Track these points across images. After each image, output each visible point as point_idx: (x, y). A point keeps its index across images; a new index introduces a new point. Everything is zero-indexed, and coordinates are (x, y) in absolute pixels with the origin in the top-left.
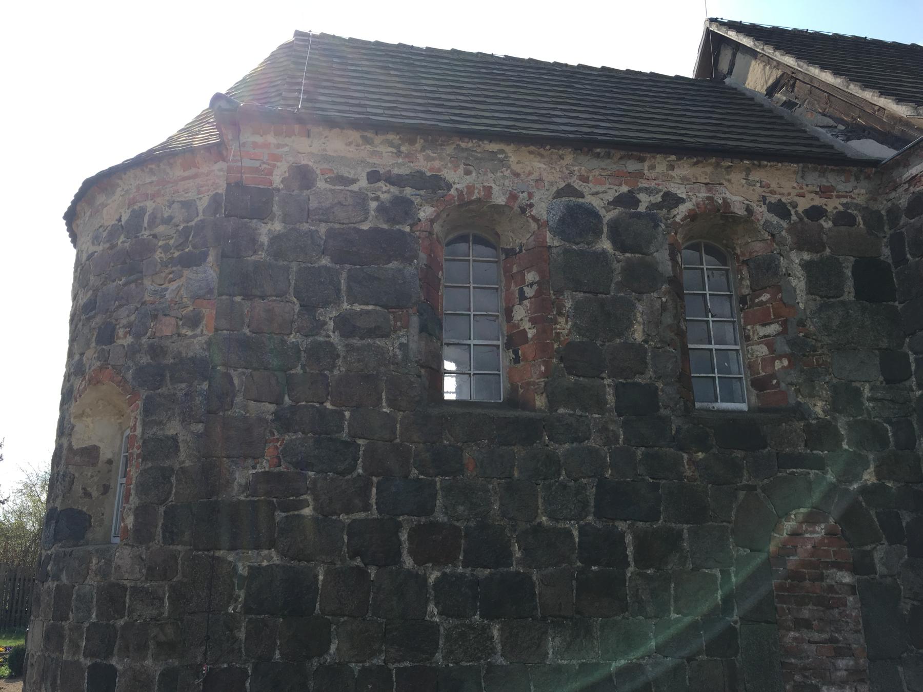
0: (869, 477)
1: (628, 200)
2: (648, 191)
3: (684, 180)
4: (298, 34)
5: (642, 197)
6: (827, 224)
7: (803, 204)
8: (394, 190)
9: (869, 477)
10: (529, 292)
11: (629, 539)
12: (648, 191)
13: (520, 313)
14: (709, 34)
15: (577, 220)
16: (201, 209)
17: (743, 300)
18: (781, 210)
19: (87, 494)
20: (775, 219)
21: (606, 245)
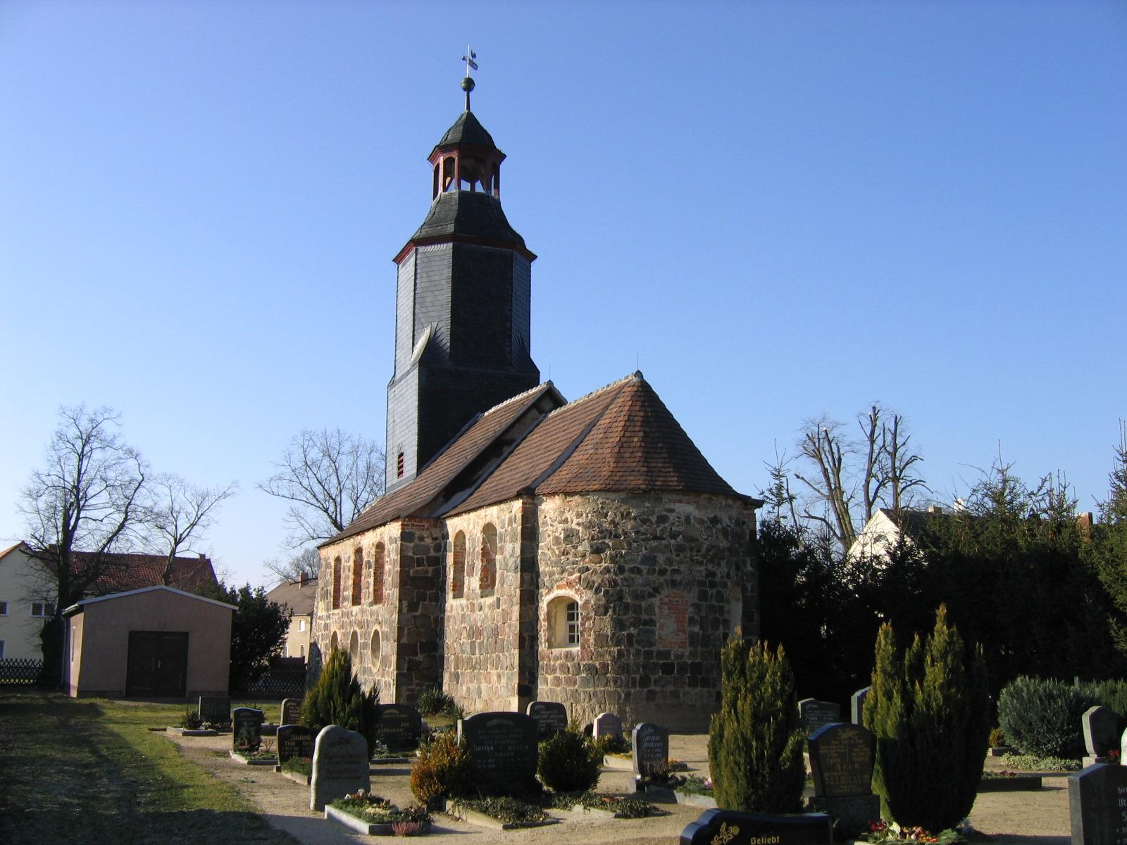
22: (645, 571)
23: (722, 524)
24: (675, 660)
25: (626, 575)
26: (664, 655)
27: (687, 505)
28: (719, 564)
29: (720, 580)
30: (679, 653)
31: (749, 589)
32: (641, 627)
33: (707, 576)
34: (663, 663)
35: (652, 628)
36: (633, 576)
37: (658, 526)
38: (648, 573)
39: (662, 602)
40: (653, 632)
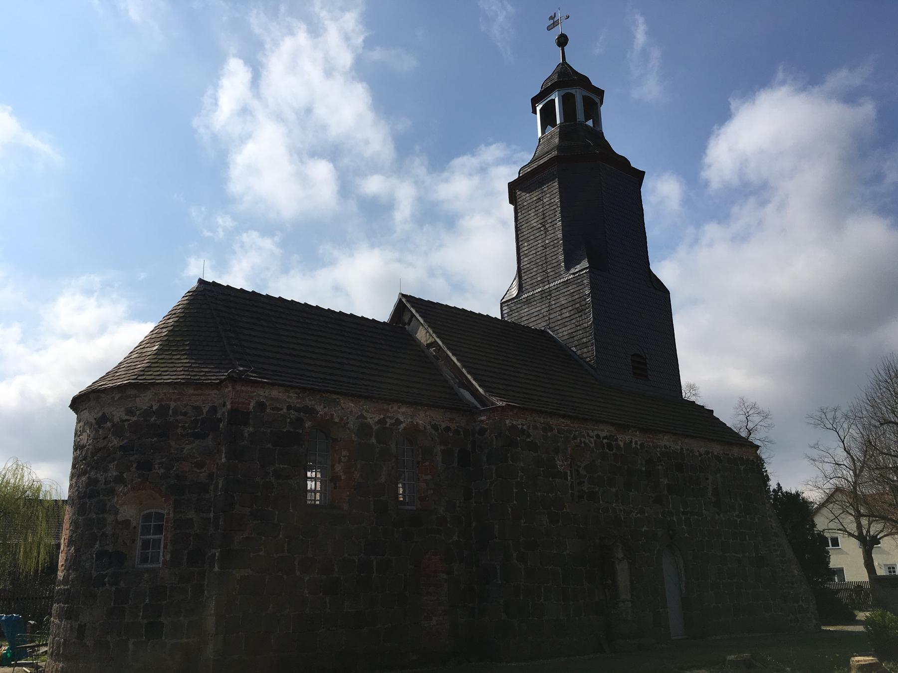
0: (455, 538)
1: (382, 422)
2: (391, 418)
3: (403, 413)
4: (201, 281)
5: (388, 420)
6: (451, 434)
7: (444, 425)
8: (296, 414)
9: (455, 538)
10: (343, 459)
11: (375, 563)
12: (391, 418)
13: (338, 468)
14: (400, 301)
15: (364, 429)
16: (205, 411)
17: (418, 463)
18: (435, 427)
19: (125, 544)
20: (433, 432)
21: (374, 441)
28: (106, 470)
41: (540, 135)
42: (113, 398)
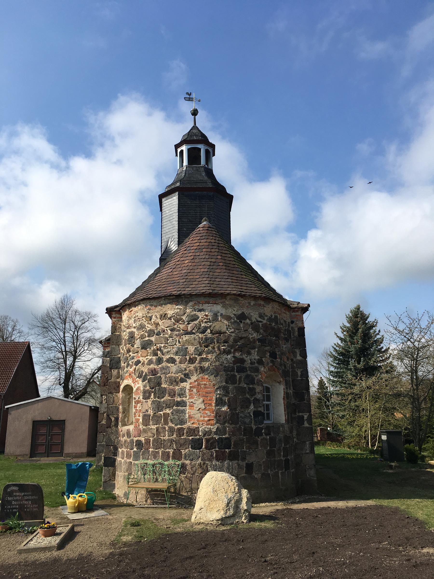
22: (178, 360)
23: (250, 320)
24: (204, 435)
25: (164, 364)
26: (193, 431)
27: (215, 305)
28: (249, 353)
29: (249, 365)
30: (206, 429)
31: (299, 373)
32: (175, 408)
33: (235, 362)
34: (193, 438)
35: (183, 408)
36: (169, 365)
37: (188, 324)
38: (180, 363)
39: (191, 385)
40: (183, 412)
41: (178, 168)
42: (249, 303)
